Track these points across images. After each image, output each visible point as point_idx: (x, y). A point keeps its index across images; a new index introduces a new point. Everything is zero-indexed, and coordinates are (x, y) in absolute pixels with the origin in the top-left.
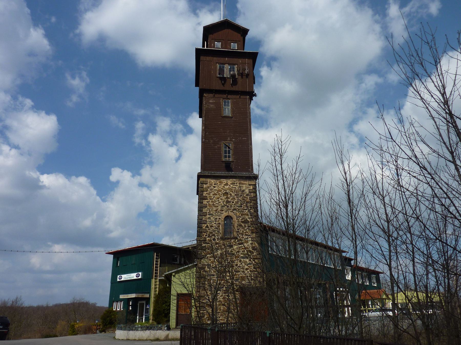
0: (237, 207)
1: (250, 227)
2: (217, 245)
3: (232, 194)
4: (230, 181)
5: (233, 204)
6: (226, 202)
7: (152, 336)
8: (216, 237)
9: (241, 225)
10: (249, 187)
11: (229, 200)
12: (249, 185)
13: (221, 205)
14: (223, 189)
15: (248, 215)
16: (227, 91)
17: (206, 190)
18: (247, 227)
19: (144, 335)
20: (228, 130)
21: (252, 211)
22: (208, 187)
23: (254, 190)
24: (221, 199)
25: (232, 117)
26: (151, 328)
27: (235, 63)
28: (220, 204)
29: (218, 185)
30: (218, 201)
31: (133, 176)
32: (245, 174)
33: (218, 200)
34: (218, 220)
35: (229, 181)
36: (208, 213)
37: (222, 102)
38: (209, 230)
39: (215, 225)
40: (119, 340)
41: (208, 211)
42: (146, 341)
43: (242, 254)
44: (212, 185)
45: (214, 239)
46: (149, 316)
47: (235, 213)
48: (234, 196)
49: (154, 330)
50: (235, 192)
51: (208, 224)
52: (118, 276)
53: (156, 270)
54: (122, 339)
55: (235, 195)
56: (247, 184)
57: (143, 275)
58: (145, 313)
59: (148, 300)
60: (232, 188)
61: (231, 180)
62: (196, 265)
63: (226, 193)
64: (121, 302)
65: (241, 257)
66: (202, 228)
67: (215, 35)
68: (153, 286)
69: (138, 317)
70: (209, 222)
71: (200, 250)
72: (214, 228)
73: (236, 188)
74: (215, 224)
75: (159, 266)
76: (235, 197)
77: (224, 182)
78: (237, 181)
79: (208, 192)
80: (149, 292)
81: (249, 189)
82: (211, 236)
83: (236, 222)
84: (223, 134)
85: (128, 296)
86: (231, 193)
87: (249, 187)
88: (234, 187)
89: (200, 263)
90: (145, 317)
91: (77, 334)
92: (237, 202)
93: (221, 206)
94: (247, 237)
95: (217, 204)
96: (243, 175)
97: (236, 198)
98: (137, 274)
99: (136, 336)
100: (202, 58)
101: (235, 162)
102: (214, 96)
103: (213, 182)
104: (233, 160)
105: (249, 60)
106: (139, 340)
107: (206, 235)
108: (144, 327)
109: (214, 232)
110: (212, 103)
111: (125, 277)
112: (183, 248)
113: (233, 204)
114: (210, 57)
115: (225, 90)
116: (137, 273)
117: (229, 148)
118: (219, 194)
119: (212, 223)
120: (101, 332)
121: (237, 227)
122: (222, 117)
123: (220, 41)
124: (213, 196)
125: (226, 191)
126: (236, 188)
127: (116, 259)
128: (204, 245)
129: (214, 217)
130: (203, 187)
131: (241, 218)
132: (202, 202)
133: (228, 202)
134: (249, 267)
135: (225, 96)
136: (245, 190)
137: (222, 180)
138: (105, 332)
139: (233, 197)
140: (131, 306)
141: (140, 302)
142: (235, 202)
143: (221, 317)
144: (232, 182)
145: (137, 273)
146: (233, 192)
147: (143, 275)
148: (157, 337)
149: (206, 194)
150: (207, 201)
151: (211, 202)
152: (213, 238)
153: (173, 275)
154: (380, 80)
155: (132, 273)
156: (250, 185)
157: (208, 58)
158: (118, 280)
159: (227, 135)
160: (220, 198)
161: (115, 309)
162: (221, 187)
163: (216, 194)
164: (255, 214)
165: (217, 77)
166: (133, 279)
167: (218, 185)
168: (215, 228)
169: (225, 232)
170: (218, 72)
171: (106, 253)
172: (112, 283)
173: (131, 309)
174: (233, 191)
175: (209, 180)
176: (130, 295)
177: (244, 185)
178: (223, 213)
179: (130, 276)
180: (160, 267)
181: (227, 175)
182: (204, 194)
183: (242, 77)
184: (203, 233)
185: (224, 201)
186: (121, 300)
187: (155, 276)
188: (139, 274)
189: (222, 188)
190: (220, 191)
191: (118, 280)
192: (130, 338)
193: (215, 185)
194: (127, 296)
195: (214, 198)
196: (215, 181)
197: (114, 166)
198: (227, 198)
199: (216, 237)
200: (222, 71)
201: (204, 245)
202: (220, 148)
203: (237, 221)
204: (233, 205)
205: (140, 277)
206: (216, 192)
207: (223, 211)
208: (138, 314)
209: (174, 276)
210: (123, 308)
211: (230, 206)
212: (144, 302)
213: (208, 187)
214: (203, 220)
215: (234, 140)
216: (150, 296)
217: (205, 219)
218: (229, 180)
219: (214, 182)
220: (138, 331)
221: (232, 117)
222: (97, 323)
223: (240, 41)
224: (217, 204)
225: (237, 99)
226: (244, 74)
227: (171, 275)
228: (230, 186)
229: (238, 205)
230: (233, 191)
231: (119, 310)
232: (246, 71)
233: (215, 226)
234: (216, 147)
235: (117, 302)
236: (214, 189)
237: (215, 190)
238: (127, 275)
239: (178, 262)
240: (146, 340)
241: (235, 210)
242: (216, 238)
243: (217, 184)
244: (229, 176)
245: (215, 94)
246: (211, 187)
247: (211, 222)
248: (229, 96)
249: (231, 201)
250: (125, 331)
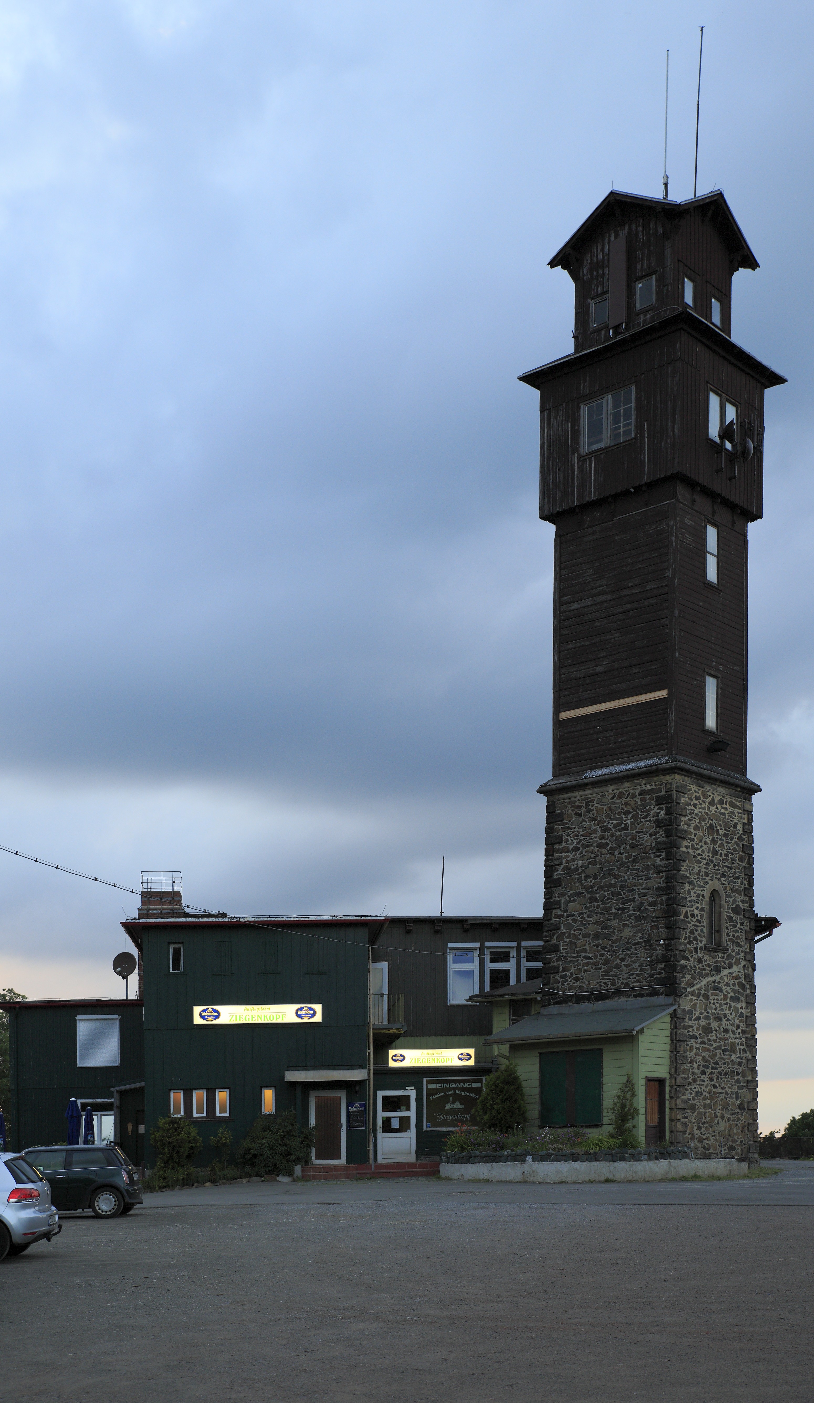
220: (641, 1162)
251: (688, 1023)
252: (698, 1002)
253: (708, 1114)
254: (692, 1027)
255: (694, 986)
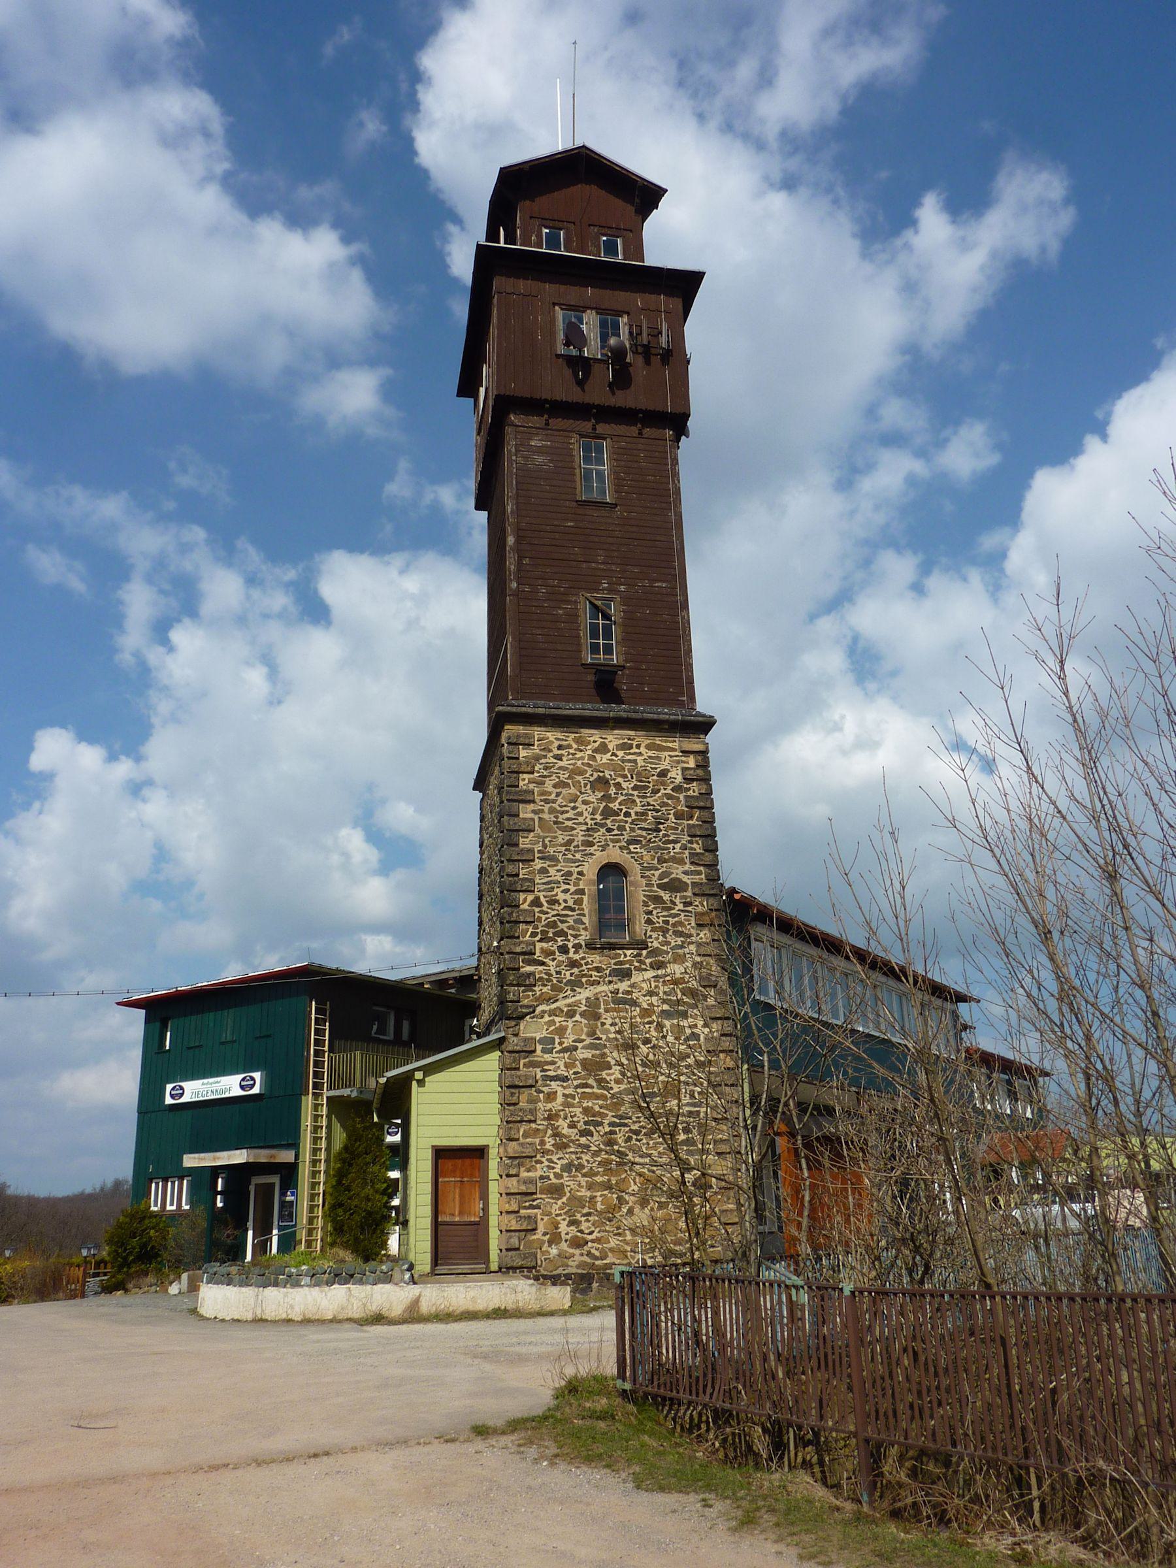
0: (644, 833)
1: (690, 904)
2: (576, 970)
3: (624, 785)
4: (613, 739)
5: (626, 822)
6: (601, 815)
7: (356, 1304)
8: (569, 941)
9: (658, 899)
10: (683, 762)
11: (611, 805)
12: (682, 752)
13: (586, 824)
14: (589, 765)
15: (681, 862)
16: (593, 406)
17: (529, 769)
18: (681, 906)
19: (324, 1303)
20: (601, 552)
21: (698, 847)
22: (537, 758)
23: (700, 772)
24: (585, 802)
25: (616, 505)
26: (352, 1276)
27: (620, 309)
28: (581, 819)
29: (571, 751)
30: (574, 808)
31: (112, 757)
32: (666, 713)
33: (572, 805)
34: (577, 879)
35: (610, 738)
36: (539, 852)
37: (576, 446)
38: (544, 917)
39: (568, 896)
40: (223, 1320)
41: (539, 847)
42: (335, 1326)
43: (664, 1002)
44: (550, 751)
45: (564, 950)
46: (295, 1231)
47: (637, 853)
48: (631, 792)
49: (361, 1282)
50: (632, 778)
51: (541, 895)
52: (169, 1087)
53: (316, 1064)
54: (234, 1320)
55: (633, 789)
56: (675, 750)
57: (266, 1082)
58: (281, 1218)
59: (289, 1173)
60: (623, 761)
61: (616, 732)
62: (502, 1040)
63: (602, 782)
64: (181, 1178)
65: (663, 1011)
66: (519, 906)
67: (544, 203)
68: (307, 1122)
69: (250, 1233)
70: (542, 887)
71: (514, 985)
72: (562, 907)
73: (637, 764)
74: (566, 891)
75: (326, 1049)
76: (633, 795)
77: (592, 739)
78: (642, 740)
79: (536, 775)
80: (294, 1145)
81: (684, 769)
82: (551, 935)
83: (637, 889)
84: (584, 565)
85: (218, 1158)
86: (620, 780)
87: (683, 762)
88: (629, 761)
89: (516, 1035)
90: (279, 1237)
91: (8, 1296)
92: (643, 814)
93: (584, 828)
94: (679, 940)
95: (568, 819)
96: (662, 717)
97: (638, 800)
98: (243, 1080)
99: (292, 1307)
100: (498, 283)
101: (629, 668)
102: (547, 424)
103: (552, 738)
104: (622, 663)
105: (671, 300)
106: (307, 1322)
107: (534, 935)
108: (324, 1273)
109: (562, 922)
110: (540, 451)
111: (195, 1090)
112: (408, 982)
113: (629, 820)
114: (529, 282)
115: (588, 404)
116: (243, 1076)
117: (606, 617)
118: (577, 784)
119: (553, 888)
120: (108, 1289)
121: (645, 904)
122: (577, 501)
123: (561, 225)
124: (555, 791)
125: (601, 774)
126: (635, 761)
127: (158, 1024)
128: (528, 969)
129: (559, 868)
130: (518, 758)
131: (657, 873)
132: (514, 811)
133: (608, 813)
134: (690, 1047)
135: (587, 426)
136: (668, 771)
137: (585, 732)
138: (126, 1291)
139: (626, 795)
140: (220, 1193)
141: (257, 1180)
142: (637, 813)
143: (598, 1229)
144: (621, 741)
145: (243, 1076)
146: (625, 776)
147: (268, 1082)
148: (373, 1308)
149: (530, 782)
150: (531, 807)
151: (550, 813)
152: (560, 943)
153: (418, 1081)
154: (918, 467)
155: (224, 1075)
156: (686, 753)
157: (522, 285)
158: (169, 1101)
159: (600, 569)
160: (580, 799)
161: (156, 1205)
162: (582, 758)
163: (566, 785)
164: (708, 858)
165: (558, 356)
166: (227, 1095)
167: (571, 751)
168: (565, 908)
169: (602, 926)
170: (561, 336)
171: (118, 1004)
172: (142, 1112)
173: (220, 1204)
174: (626, 772)
175: (537, 732)
176: (225, 1154)
177: (666, 754)
178: (591, 854)
179: (214, 1087)
180: (331, 1050)
181: (605, 714)
182: (521, 783)
183: (648, 362)
184: (522, 926)
185: (594, 809)
186: (192, 1171)
187: (315, 1086)
188: (253, 1079)
189: (586, 761)
190: (581, 773)
191: (169, 1101)
192: (267, 1316)
193: (560, 752)
194: (214, 1159)
195: (560, 800)
196: (560, 736)
197: (52, 723)
198: (606, 798)
199: (569, 941)
200: (574, 336)
201: (528, 969)
202: (573, 617)
203: (644, 881)
204: (627, 826)
205: (256, 1090)
206: (566, 776)
207: (591, 844)
208: (250, 1224)
209: (421, 1083)
210: (191, 1202)
211: (619, 828)
212: (275, 1180)
213: (537, 758)
214: (521, 876)
215: (622, 588)
216: (297, 1156)
217: (529, 873)
218: (609, 732)
219: (557, 739)
220: (300, 1289)
221: (616, 505)
222: (85, 1257)
223: (631, 231)
224: (568, 819)
225: (628, 439)
226: (653, 351)
227: (408, 1078)
228: (614, 754)
229: (645, 825)
230: (626, 772)
231: (174, 1208)
232: (664, 341)
233: (565, 901)
234: (561, 612)
235: (165, 1180)
236: (557, 766)
237: (560, 768)
238: (205, 1081)
239: (390, 1036)
240: (334, 1321)
241: (631, 842)
242: (570, 945)
243: (570, 747)
244: (613, 718)
245: (550, 418)
246: (545, 757)
247: (550, 885)
248: (601, 428)
249: (621, 810)
250: (244, 1289)
251: (542, 1057)
252: (570, 1024)
253: (599, 1199)
254: (553, 1063)
255: (557, 1001)
